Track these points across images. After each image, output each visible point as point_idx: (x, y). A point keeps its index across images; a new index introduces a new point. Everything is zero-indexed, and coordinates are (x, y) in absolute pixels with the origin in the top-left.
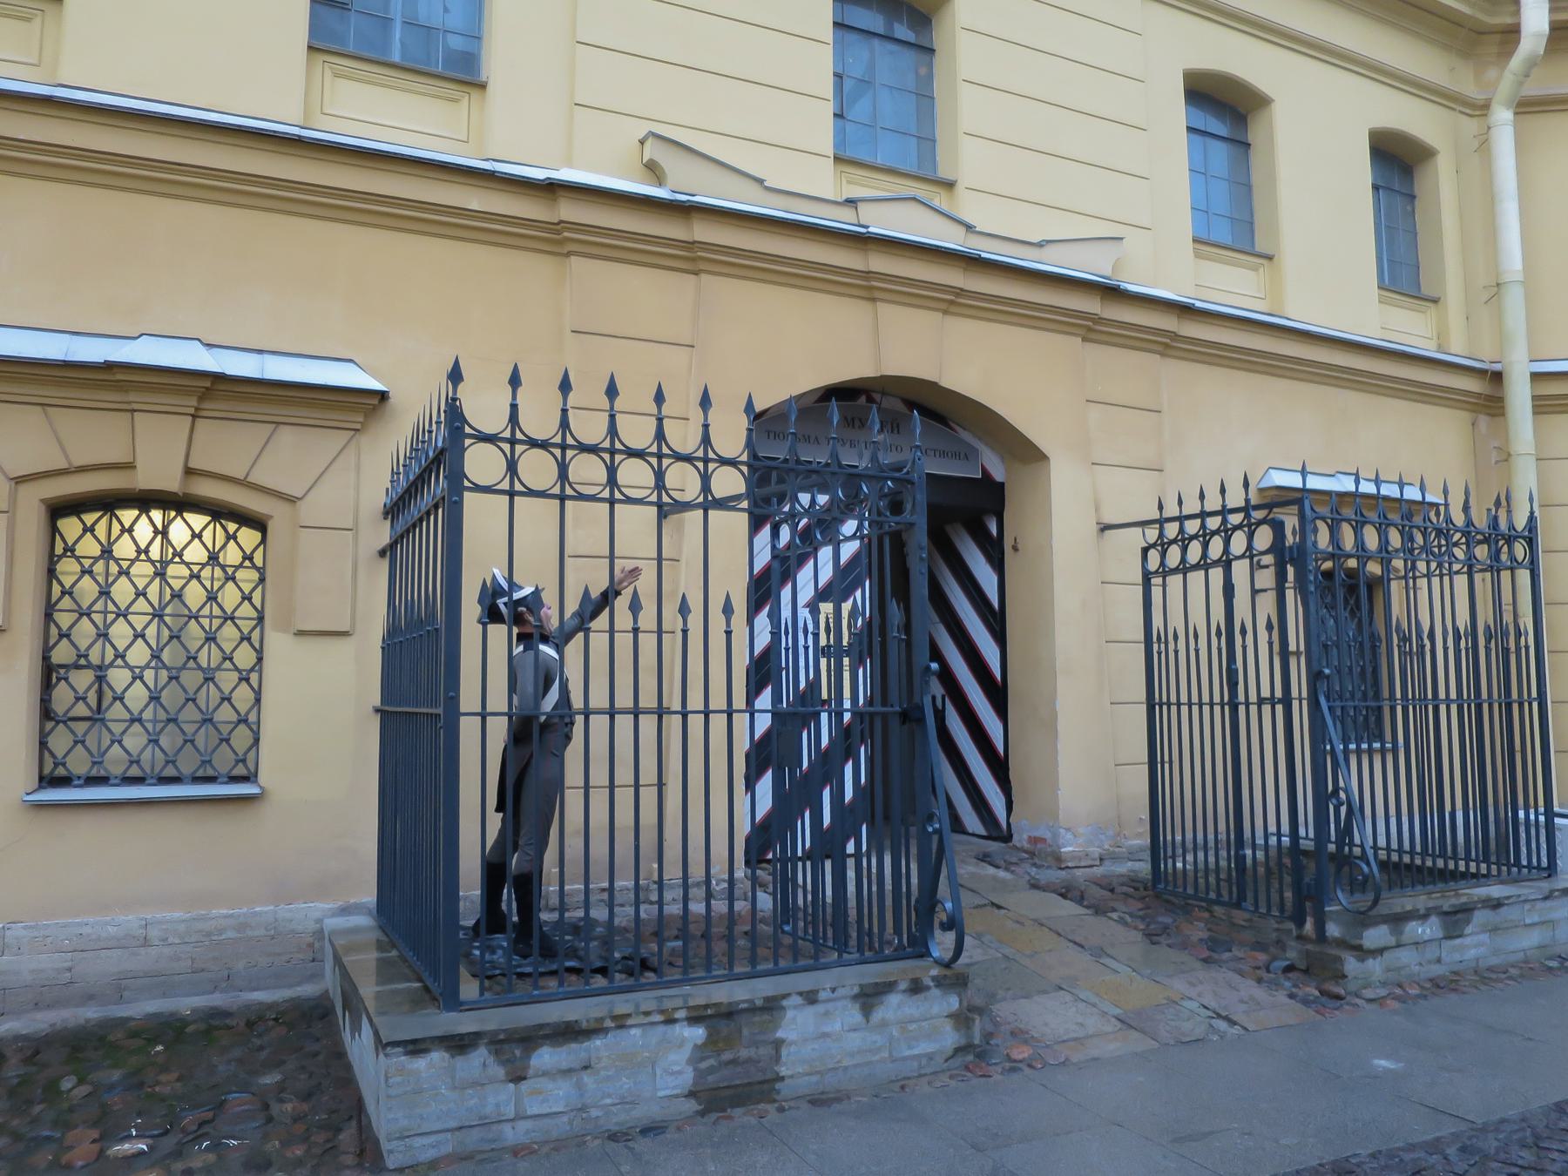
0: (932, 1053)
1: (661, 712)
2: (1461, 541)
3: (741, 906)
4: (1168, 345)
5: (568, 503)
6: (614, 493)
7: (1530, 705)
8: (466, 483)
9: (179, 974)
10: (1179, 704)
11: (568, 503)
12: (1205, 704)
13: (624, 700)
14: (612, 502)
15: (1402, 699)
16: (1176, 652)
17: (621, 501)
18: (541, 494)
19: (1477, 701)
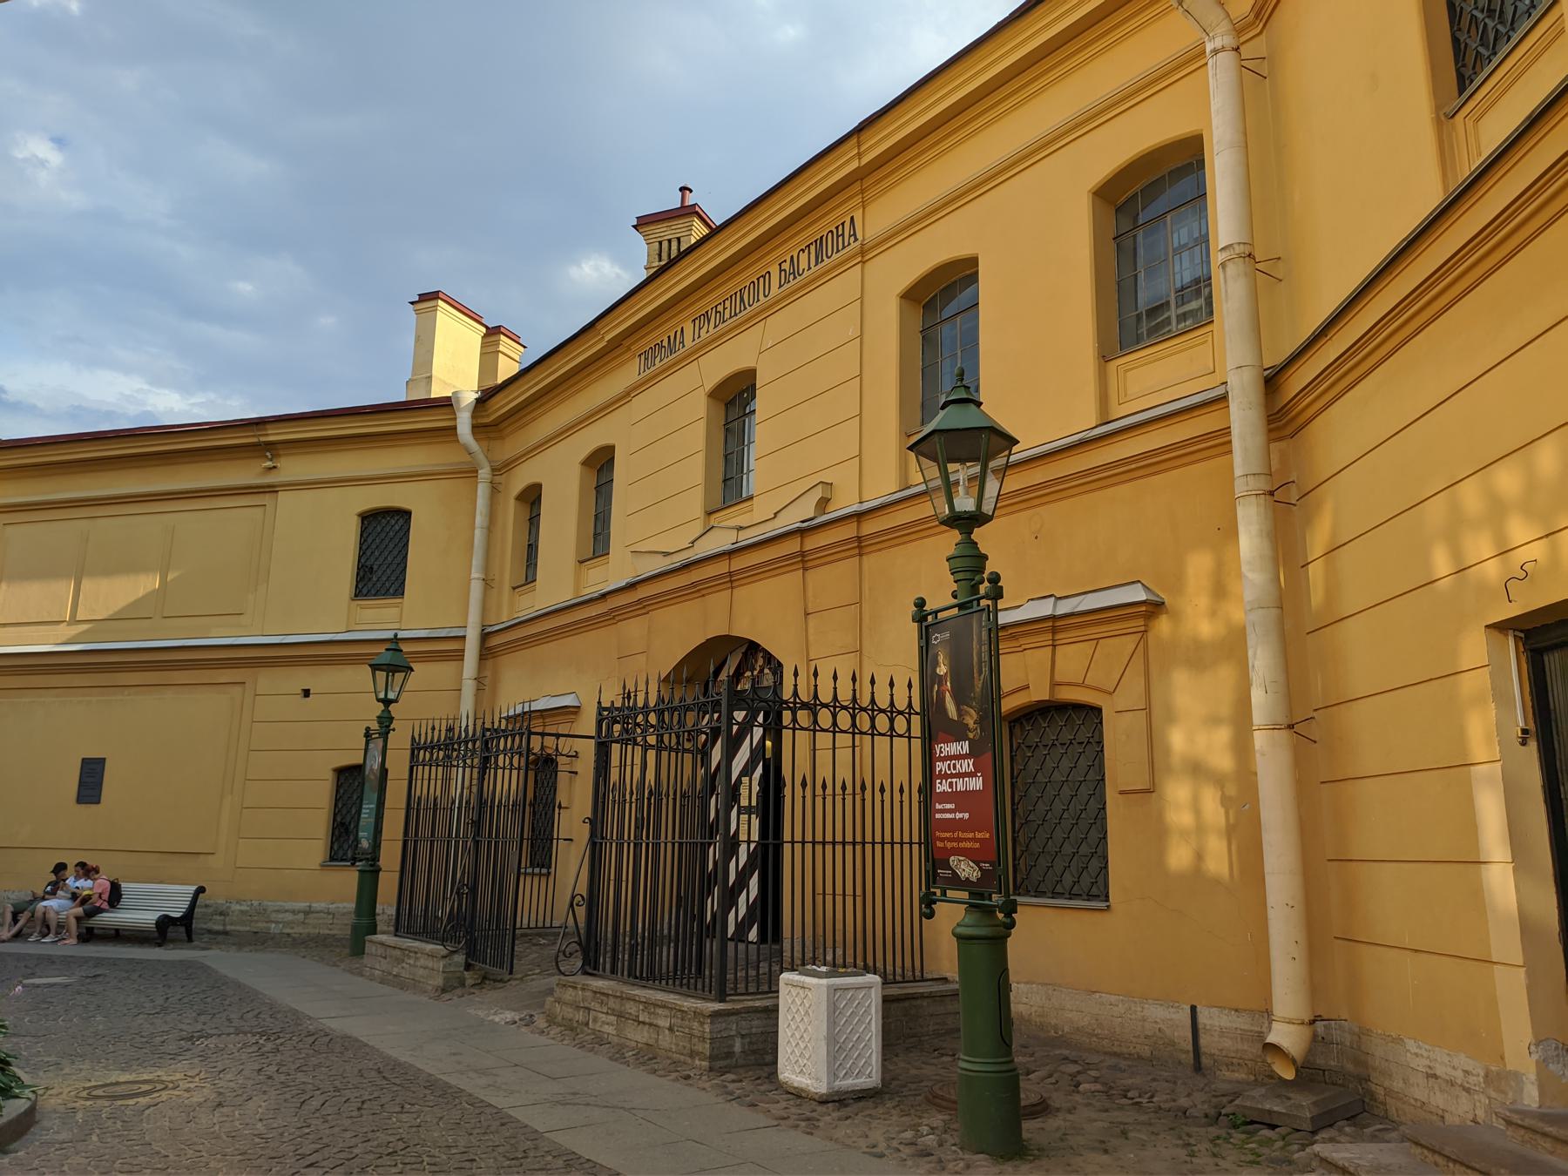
0: (1371, 1142)
1: (854, 843)
2: (819, 707)
3: (37, 1137)
4: (643, 606)
5: (837, 734)
6: (873, 732)
7: (611, 844)
8: (734, 722)
9: (592, 1074)
10: (864, 843)
11: (837, 734)
12: (788, 842)
13: (839, 838)
14: (834, 732)
15: (456, 837)
16: (883, 801)
17: (818, 731)
18: (826, 731)
19: (766, 842)
